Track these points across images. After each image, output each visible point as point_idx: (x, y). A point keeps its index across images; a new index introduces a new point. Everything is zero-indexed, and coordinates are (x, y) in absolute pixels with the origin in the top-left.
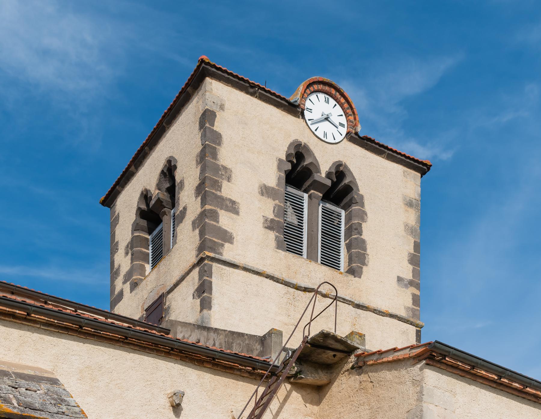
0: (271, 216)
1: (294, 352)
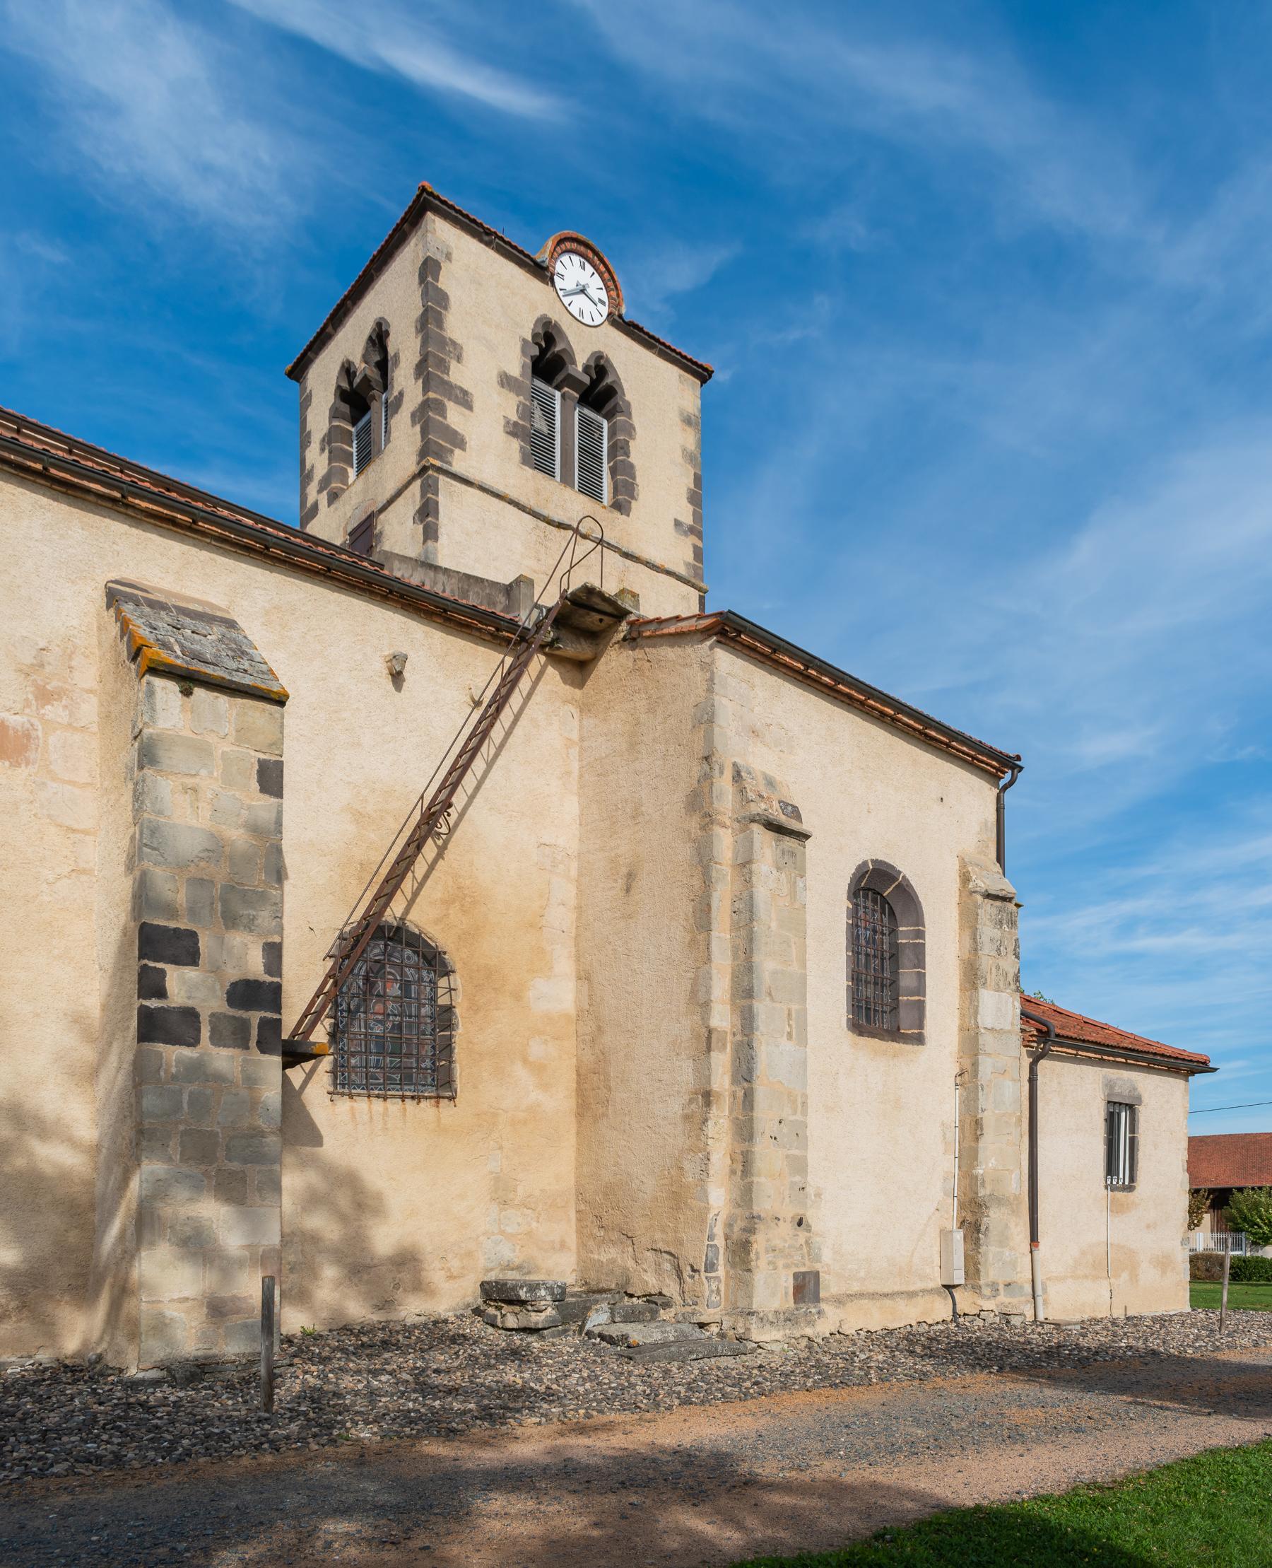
0: (514, 417)
1: (549, 610)
